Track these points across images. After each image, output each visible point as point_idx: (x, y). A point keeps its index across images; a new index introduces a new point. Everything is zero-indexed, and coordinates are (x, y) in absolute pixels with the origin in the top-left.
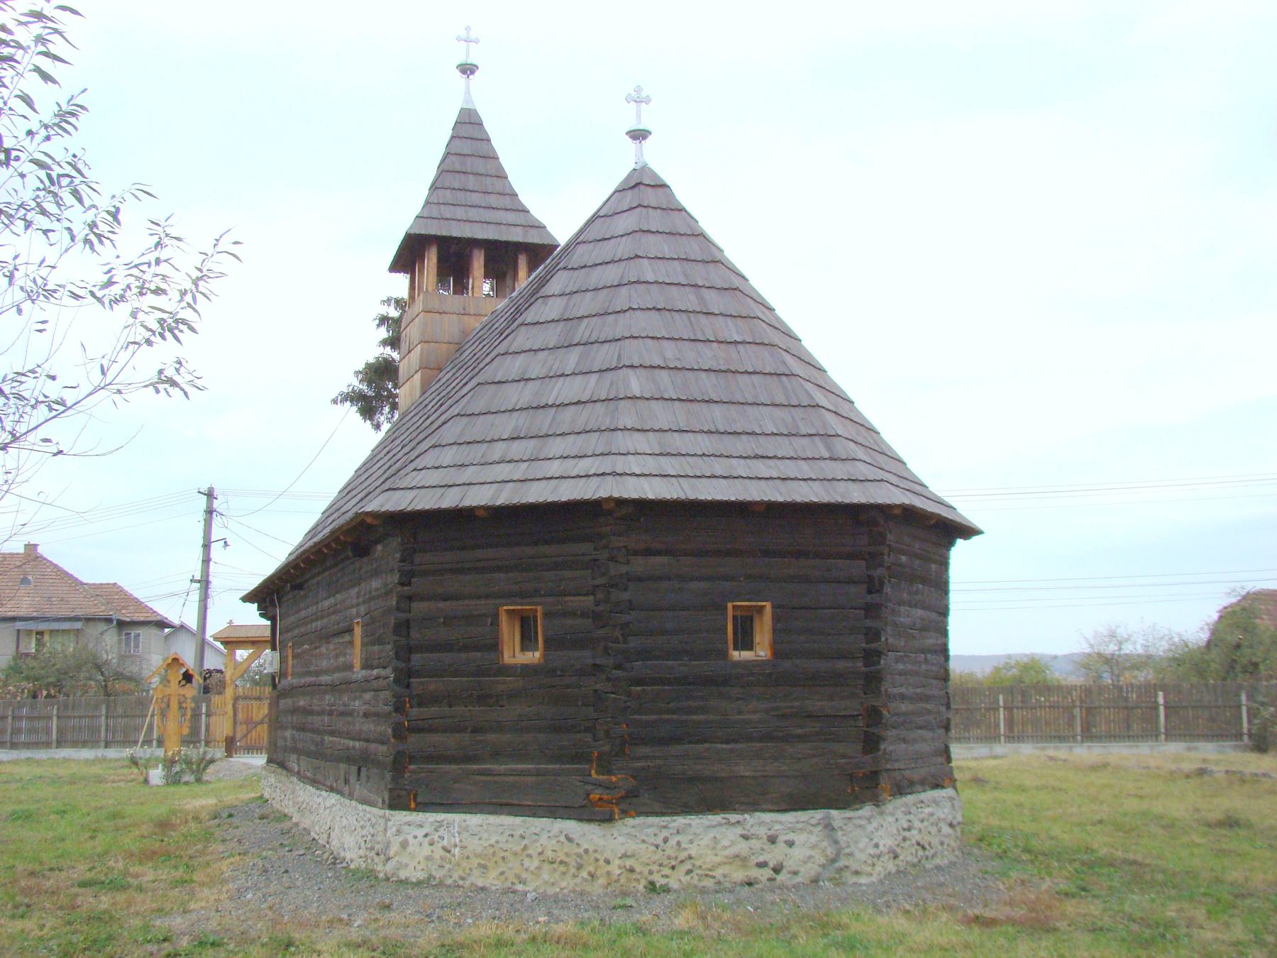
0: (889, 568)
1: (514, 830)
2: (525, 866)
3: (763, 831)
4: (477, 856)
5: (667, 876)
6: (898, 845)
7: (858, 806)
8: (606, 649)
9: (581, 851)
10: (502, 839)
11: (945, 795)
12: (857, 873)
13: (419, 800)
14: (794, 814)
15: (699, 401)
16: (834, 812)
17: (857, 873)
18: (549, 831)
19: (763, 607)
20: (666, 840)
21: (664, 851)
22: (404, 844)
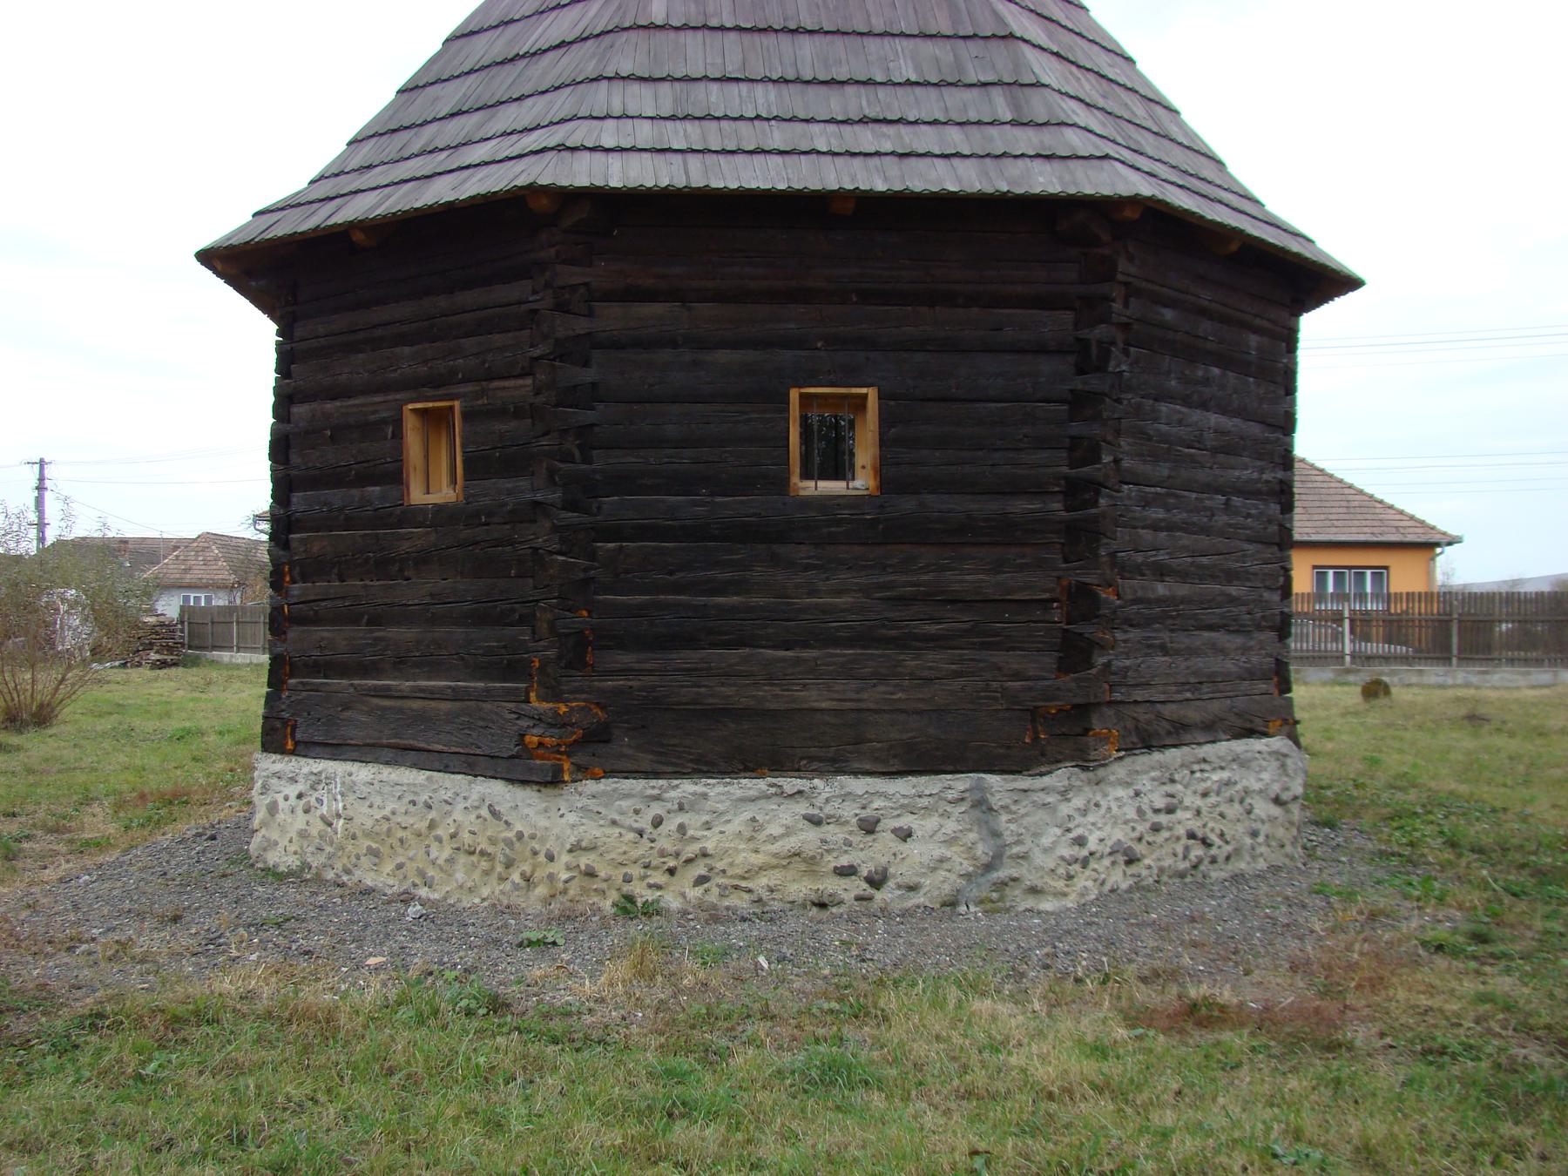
0: (1125, 327)
1: (416, 793)
2: (433, 856)
3: (850, 811)
4: (368, 834)
5: (659, 887)
6: (1140, 839)
7: (1043, 769)
8: (552, 473)
9: (511, 835)
10: (401, 807)
11: (1265, 749)
12: (1034, 891)
13: (298, 736)
14: (912, 780)
15: (776, 31)
16: (993, 780)
17: (1034, 891)
18: (465, 798)
19: (865, 396)
20: (657, 822)
21: (653, 841)
22: (273, 809)
